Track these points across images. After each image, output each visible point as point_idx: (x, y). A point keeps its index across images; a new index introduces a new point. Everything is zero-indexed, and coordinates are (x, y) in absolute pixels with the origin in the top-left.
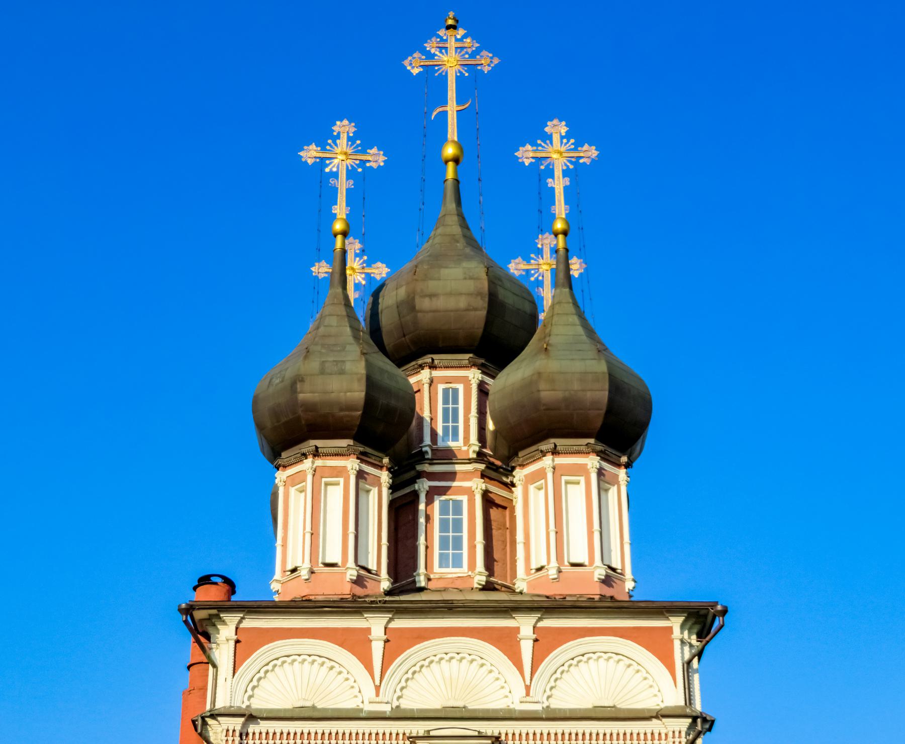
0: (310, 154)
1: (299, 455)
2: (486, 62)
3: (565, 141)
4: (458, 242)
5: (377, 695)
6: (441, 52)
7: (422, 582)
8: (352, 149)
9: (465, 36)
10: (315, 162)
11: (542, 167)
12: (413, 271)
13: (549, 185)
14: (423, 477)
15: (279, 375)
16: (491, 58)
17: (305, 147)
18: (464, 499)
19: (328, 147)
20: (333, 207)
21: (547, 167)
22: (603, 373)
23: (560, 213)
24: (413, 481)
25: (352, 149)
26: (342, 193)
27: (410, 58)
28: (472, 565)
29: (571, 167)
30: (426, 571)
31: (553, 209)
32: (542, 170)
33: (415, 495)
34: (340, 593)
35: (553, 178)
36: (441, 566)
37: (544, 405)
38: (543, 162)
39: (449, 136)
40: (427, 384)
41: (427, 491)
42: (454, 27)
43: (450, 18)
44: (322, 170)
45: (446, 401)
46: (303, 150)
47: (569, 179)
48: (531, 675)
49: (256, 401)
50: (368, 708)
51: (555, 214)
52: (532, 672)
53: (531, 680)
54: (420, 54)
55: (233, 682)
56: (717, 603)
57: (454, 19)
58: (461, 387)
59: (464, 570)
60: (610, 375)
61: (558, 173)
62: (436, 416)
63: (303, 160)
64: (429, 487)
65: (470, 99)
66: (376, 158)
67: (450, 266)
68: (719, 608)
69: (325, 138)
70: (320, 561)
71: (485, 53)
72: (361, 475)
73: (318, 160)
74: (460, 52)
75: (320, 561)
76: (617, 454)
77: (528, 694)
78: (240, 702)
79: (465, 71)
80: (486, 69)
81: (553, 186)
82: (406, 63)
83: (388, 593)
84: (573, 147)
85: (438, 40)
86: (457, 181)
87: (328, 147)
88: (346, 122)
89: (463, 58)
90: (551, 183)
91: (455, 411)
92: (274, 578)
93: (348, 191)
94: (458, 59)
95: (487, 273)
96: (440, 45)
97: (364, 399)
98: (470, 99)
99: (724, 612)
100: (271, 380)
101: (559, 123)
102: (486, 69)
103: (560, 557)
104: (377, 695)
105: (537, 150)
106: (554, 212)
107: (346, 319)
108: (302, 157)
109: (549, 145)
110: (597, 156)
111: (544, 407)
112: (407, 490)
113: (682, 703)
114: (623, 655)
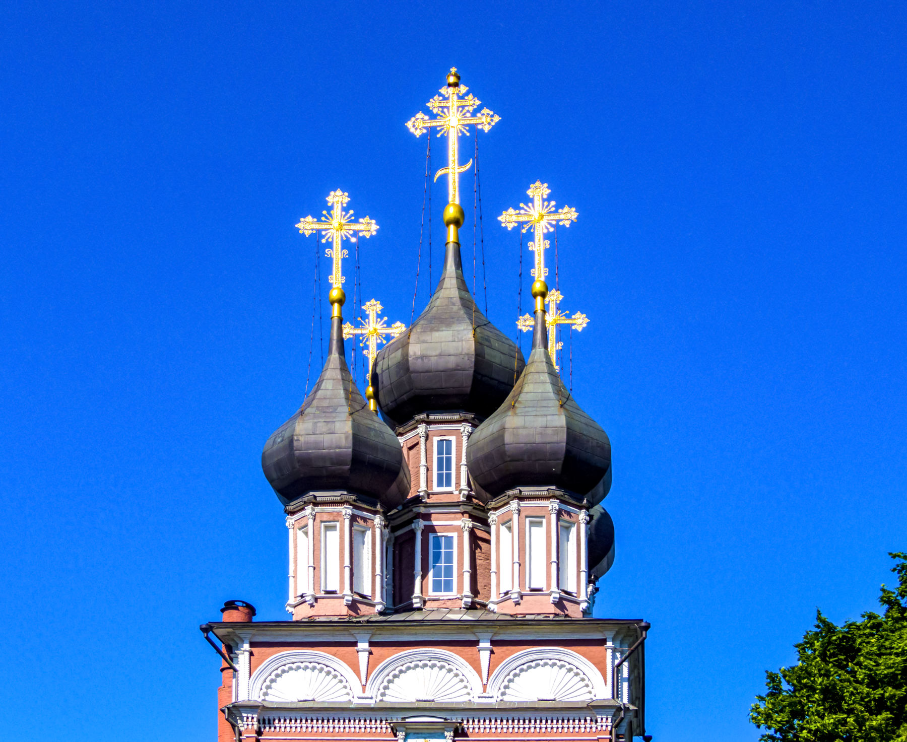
0: (307, 225)
1: (302, 503)
2: (487, 121)
3: (546, 203)
4: (454, 304)
5: (364, 691)
6: (443, 112)
7: (417, 603)
8: (346, 220)
9: (467, 94)
10: (312, 233)
11: (524, 231)
12: (407, 336)
13: (530, 249)
14: (419, 518)
15: (280, 435)
16: (492, 116)
17: (302, 220)
18: (455, 535)
19: (323, 219)
20: (330, 277)
21: (529, 230)
22: (562, 427)
23: (540, 276)
24: (410, 521)
25: (346, 220)
26: (337, 264)
27: (413, 119)
28: (460, 589)
29: (552, 230)
30: (422, 595)
31: (532, 272)
32: (523, 234)
33: (413, 533)
34: (339, 614)
35: (534, 241)
36: (434, 591)
37: (509, 456)
38: (525, 226)
39: (450, 199)
40: (424, 438)
41: (423, 530)
42: (456, 85)
43: (452, 75)
44: (319, 241)
45: (440, 452)
46: (300, 222)
47: (549, 242)
48: (488, 676)
49: (264, 459)
50: (356, 702)
51: (534, 277)
52: (488, 674)
53: (488, 680)
54: (423, 114)
55: (250, 683)
56: (642, 620)
57: (456, 75)
58: (453, 439)
59: (454, 594)
60: (568, 428)
61: (539, 234)
62: (432, 465)
63: (301, 232)
64: (425, 526)
65: (471, 160)
66: (369, 227)
67: (441, 329)
68: (643, 624)
69: (320, 210)
70: (323, 588)
71: (485, 111)
72: (353, 519)
73: (314, 232)
74: (461, 111)
75: (323, 588)
76: (399, 519)
77: (485, 691)
78: (256, 697)
79: (467, 130)
80: (487, 129)
81: (534, 249)
82: (409, 124)
83: (381, 613)
84: (553, 209)
85: (441, 98)
86: (457, 244)
87: (323, 219)
88: (339, 192)
89: (465, 117)
90: (532, 246)
91: (449, 460)
92: (288, 603)
93: (344, 260)
94: (460, 118)
95: (474, 335)
96: (442, 105)
97: (351, 455)
98: (471, 160)
99: (647, 628)
100: (275, 439)
101: (542, 185)
102: (487, 129)
103: (521, 584)
104: (364, 691)
105: (519, 214)
106: (533, 275)
107: (341, 383)
108: (299, 229)
109: (532, 208)
110: (576, 218)
111: (509, 459)
113: (610, 696)
114: (565, 661)
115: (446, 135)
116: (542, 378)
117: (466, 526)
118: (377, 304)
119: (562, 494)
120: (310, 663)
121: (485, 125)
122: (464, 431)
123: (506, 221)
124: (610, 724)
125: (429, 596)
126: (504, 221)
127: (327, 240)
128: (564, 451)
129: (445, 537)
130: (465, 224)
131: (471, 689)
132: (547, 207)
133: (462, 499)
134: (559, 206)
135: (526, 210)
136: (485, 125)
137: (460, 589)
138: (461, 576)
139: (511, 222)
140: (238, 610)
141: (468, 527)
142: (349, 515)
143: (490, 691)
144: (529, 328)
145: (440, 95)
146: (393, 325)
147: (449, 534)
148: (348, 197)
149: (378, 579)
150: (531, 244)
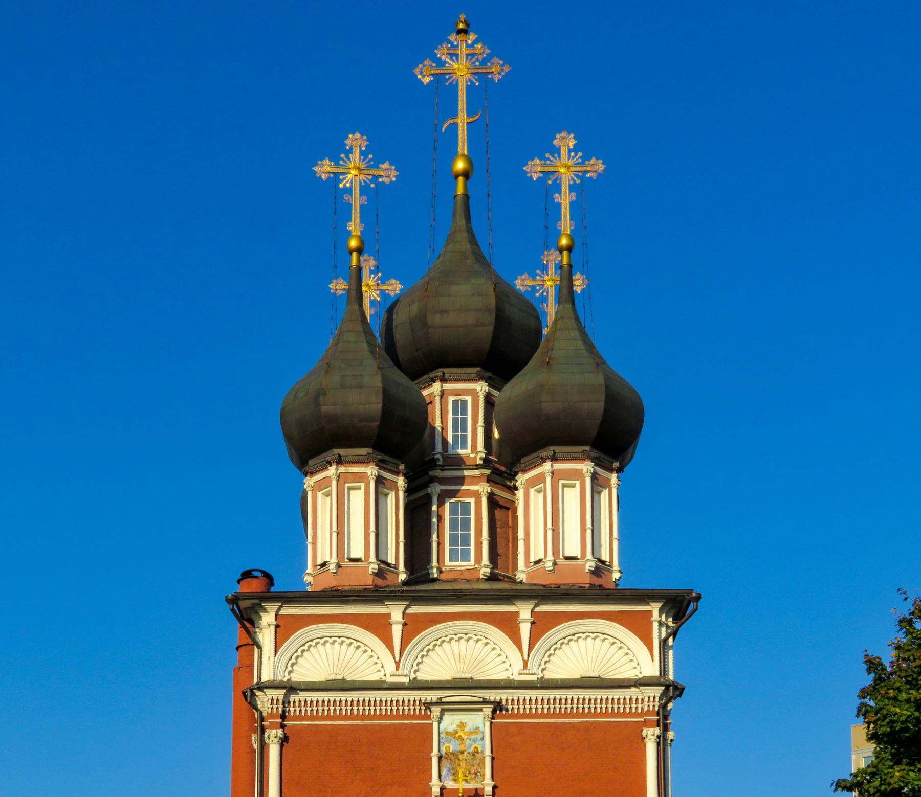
1: (324, 463)
4: (466, 258)
14: (435, 482)
15: (303, 389)
18: (472, 501)
21: (555, 182)
23: (566, 229)
24: (426, 485)
28: (478, 559)
29: (578, 181)
34: (364, 584)
40: (438, 397)
43: (461, 22)
44: (336, 186)
55: (276, 660)
58: (469, 399)
60: (607, 387)
68: (694, 594)
69: (338, 152)
71: (496, 60)
74: (471, 60)
75: (346, 556)
87: (341, 162)
88: (358, 135)
90: (558, 198)
91: (464, 421)
94: (469, 66)
100: (297, 393)
107: (363, 335)
112: (421, 493)
115: (454, 83)
116: (572, 334)
117: (485, 491)
118: (370, 259)
119: (597, 456)
120: (556, 643)
121: (496, 74)
122: (481, 390)
123: (531, 171)
124: (657, 704)
125: (446, 566)
126: (529, 170)
127: (345, 185)
128: (602, 411)
129: (463, 503)
130: (473, 177)
131: (510, 666)
132: (573, 158)
133: (479, 462)
134: (586, 158)
135: (551, 161)
136: (496, 74)
137: (478, 559)
138: (479, 544)
139: (537, 173)
140: (258, 578)
141: (487, 492)
142: (375, 476)
143: (533, 666)
144: (527, 287)
145: (449, 42)
146: (387, 282)
147: (467, 500)
148: (367, 140)
149: (615, 544)
150: (557, 196)
